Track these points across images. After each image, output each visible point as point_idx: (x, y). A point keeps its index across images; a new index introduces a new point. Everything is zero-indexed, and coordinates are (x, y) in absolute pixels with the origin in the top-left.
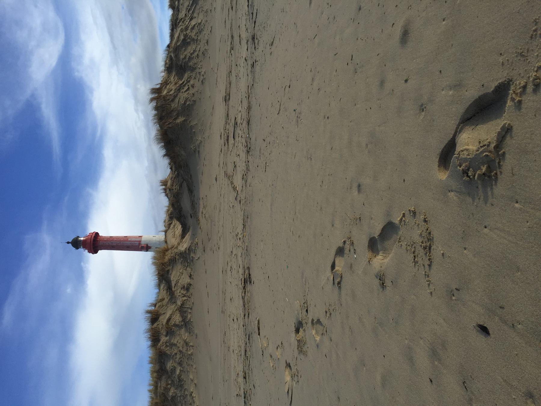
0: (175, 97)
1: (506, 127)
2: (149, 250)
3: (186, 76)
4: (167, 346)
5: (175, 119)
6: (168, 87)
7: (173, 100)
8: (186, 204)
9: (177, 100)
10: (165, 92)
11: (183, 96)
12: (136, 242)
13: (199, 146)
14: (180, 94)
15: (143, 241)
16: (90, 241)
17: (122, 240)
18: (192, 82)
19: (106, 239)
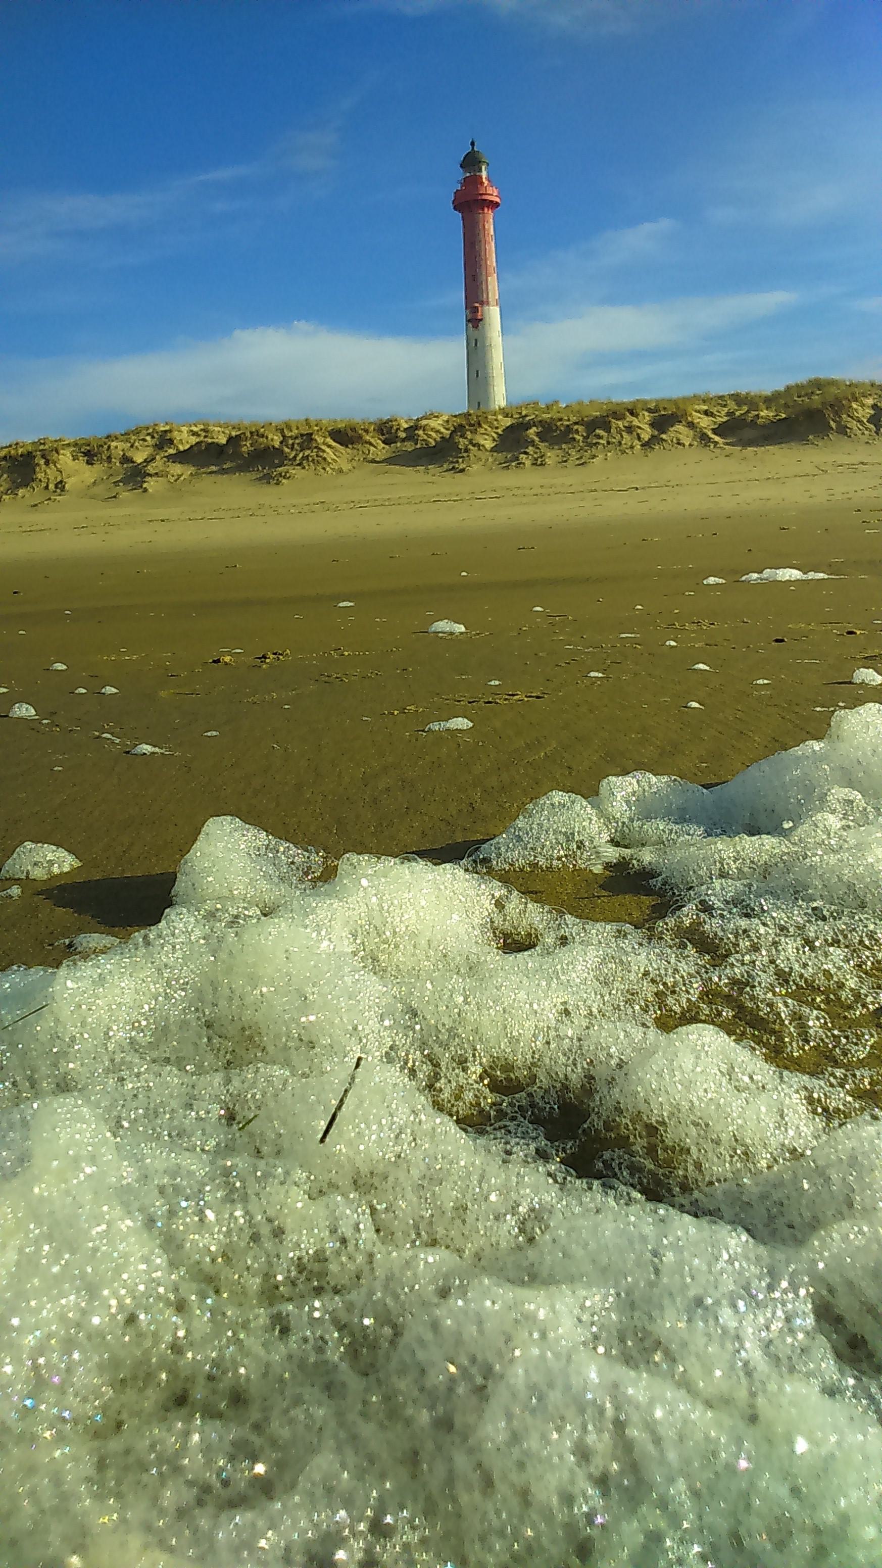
0: (852, 418)
1: (388, 1490)
2: (470, 325)
3: (872, 426)
4: (616, 428)
5: (833, 420)
6: (860, 408)
7: (849, 416)
8: (748, 433)
9: (849, 419)
10: (854, 405)
11: (853, 424)
12: (485, 296)
13: (813, 444)
14: (855, 422)
15: (489, 309)
16: (481, 192)
17: (488, 263)
18: (866, 432)
19: (486, 227)
